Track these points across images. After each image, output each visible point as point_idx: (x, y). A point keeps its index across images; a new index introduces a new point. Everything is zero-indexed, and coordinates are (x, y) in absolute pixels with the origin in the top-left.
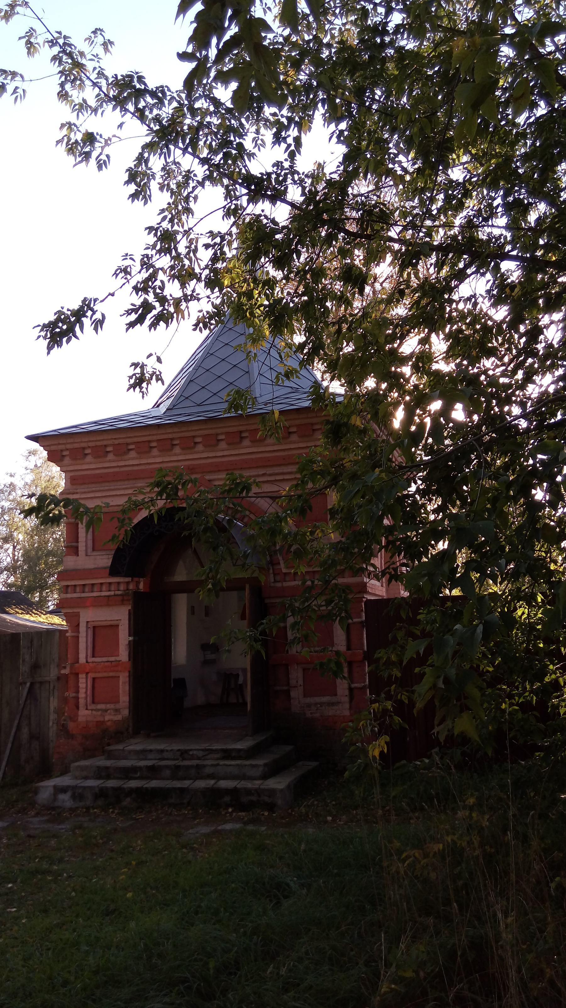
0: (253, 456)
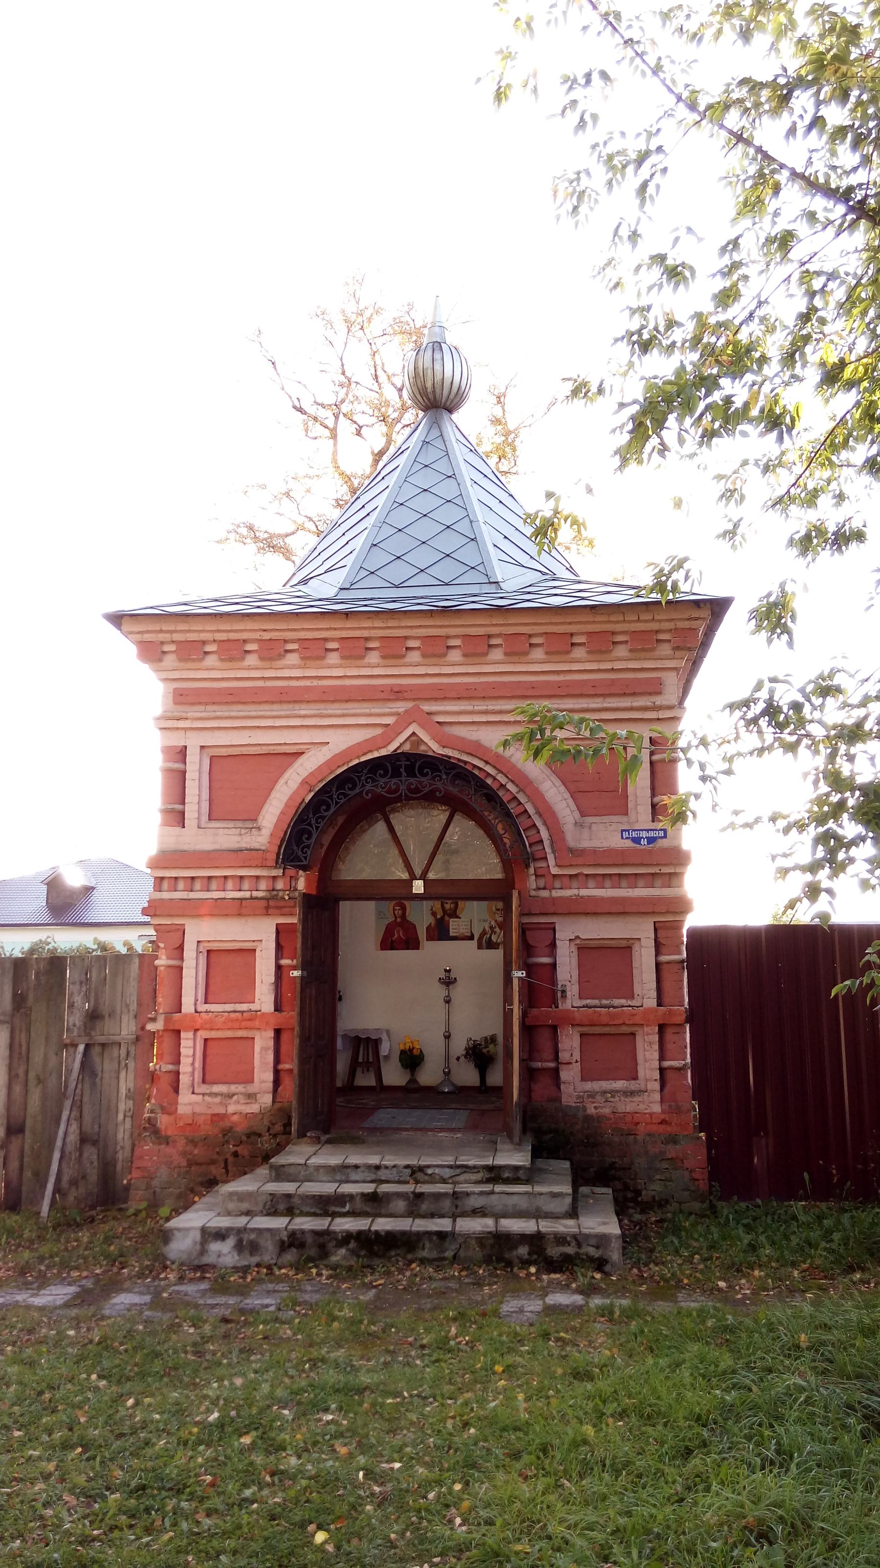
0: (561, 678)
